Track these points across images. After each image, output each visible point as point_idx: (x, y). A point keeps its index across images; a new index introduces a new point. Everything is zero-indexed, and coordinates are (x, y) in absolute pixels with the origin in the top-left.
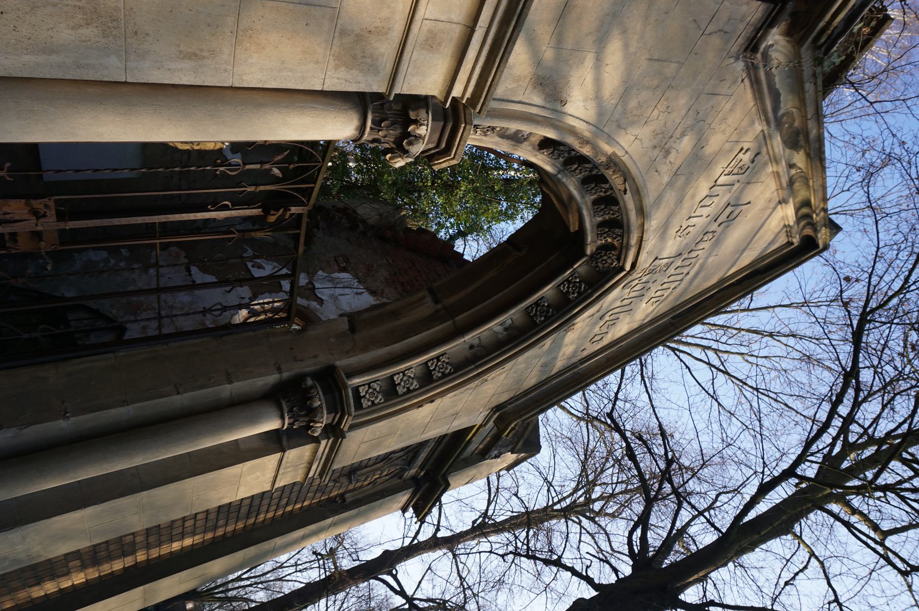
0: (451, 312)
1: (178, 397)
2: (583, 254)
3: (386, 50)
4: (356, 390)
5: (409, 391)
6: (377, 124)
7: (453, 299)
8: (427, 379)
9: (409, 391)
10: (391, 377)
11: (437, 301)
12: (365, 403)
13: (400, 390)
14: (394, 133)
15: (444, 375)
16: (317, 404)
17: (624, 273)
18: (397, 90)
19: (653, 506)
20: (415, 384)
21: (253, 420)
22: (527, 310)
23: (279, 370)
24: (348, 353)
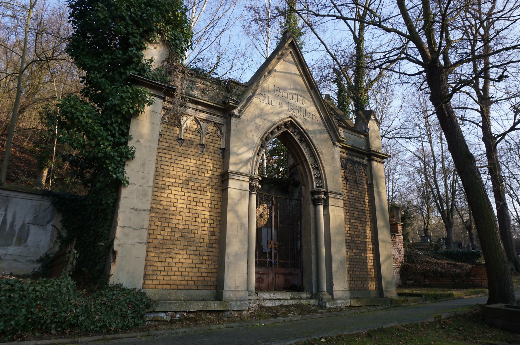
0: (302, 162)
1: (311, 226)
2: (287, 131)
3: (243, 192)
4: (317, 187)
5: (320, 174)
6: (254, 191)
7: (299, 160)
8: (318, 169)
9: (320, 174)
10: (316, 178)
11: (299, 164)
12: (321, 185)
13: (319, 176)
14: (255, 188)
15: (317, 164)
16: (317, 197)
17: (292, 120)
18: (248, 190)
19: (433, 36)
20: (318, 172)
21: (319, 211)
22: (301, 143)
23: (310, 204)
24: (309, 188)
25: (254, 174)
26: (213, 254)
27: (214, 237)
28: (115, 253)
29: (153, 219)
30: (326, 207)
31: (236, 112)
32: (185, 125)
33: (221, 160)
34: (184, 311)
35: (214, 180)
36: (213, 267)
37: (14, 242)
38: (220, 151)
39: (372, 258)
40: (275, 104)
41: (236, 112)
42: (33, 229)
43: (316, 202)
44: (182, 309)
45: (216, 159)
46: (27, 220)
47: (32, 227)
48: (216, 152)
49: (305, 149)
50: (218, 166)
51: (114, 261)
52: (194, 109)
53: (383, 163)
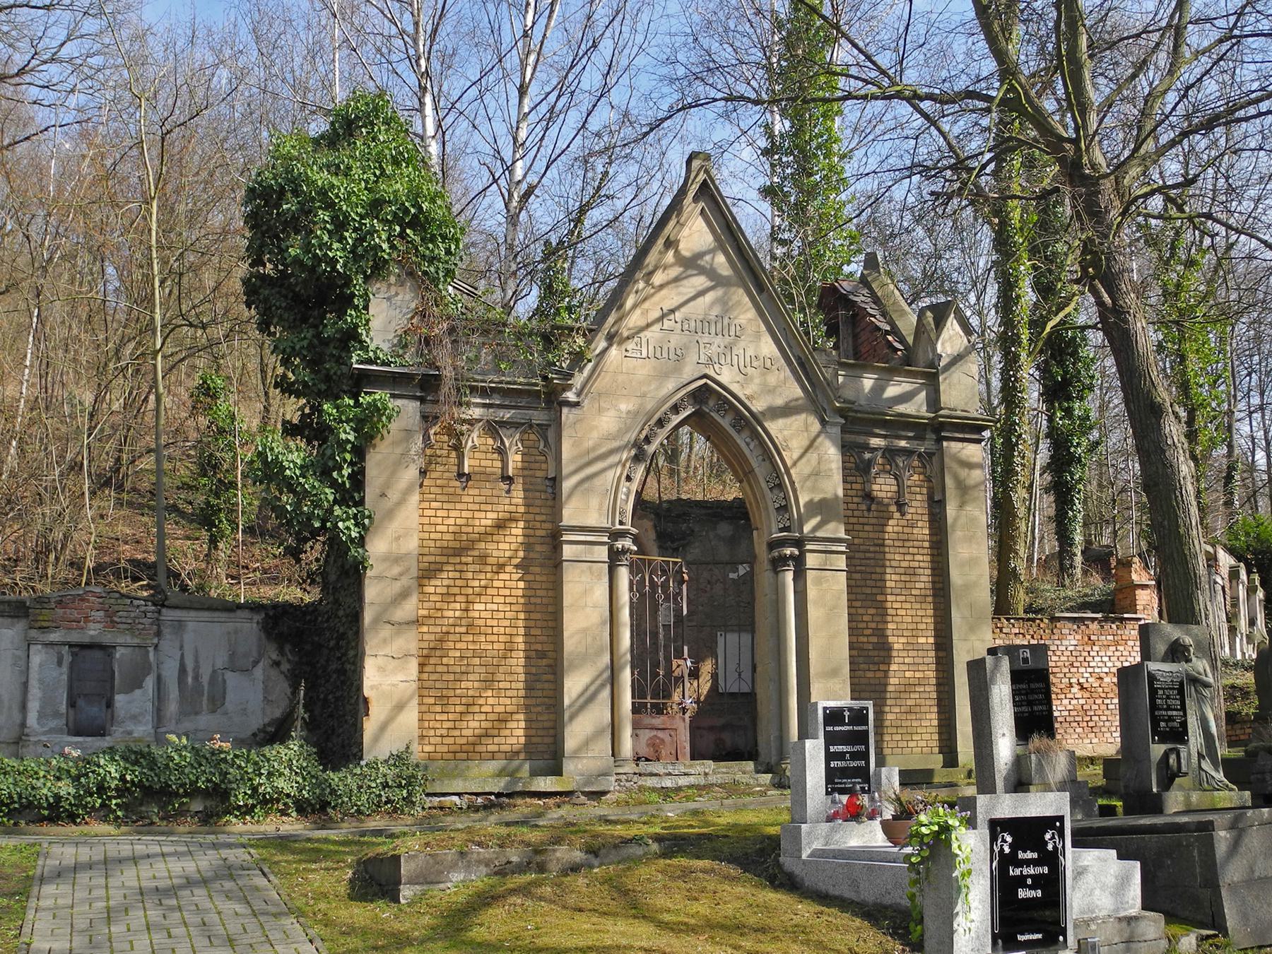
20: (782, 495)
21: (784, 585)
22: (738, 432)
25: (621, 523)
26: (545, 693)
27: (545, 662)
28: (366, 701)
29: (856, 660)
30: (800, 575)
31: (571, 396)
32: (470, 444)
33: (550, 503)
34: (491, 794)
35: (538, 548)
36: (545, 717)
37: (205, 707)
38: (547, 483)
39: (934, 681)
40: (665, 355)
41: (571, 396)
42: (232, 679)
43: (778, 564)
44: (487, 790)
45: (538, 502)
46: (219, 664)
47: (229, 676)
48: (539, 488)
49: (748, 444)
50: (544, 518)
51: (367, 715)
52: (484, 406)
53: (979, 441)
